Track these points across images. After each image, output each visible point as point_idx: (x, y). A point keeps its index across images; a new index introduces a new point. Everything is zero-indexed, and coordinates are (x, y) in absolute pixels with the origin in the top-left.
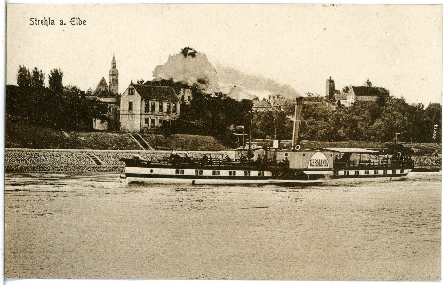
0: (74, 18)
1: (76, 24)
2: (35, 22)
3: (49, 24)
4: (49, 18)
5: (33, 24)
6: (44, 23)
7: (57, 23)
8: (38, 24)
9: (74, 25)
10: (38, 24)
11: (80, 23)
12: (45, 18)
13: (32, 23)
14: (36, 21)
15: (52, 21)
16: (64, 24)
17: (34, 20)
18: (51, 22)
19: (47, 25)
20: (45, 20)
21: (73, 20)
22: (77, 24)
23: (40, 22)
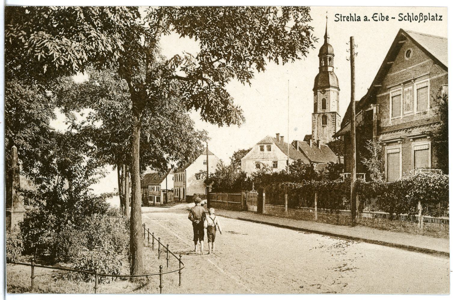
0: (377, 14)
1: (378, 20)
2: (340, 18)
3: (413, 20)
4: (355, 14)
5: (402, 20)
6: (349, 19)
7: (362, 18)
8: (344, 20)
9: (377, 21)
10: (344, 20)
11: (383, 18)
12: (350, 14)
13: (337, 19)
14: (341, 17)
15: (432, 16)
16: (368, 19)
17: (339, 16)
18: (357, 18)
19: (411, 21)
20: (351, 17)
21: (375, 15)
22: (380, 20)
23: (345, 19)
